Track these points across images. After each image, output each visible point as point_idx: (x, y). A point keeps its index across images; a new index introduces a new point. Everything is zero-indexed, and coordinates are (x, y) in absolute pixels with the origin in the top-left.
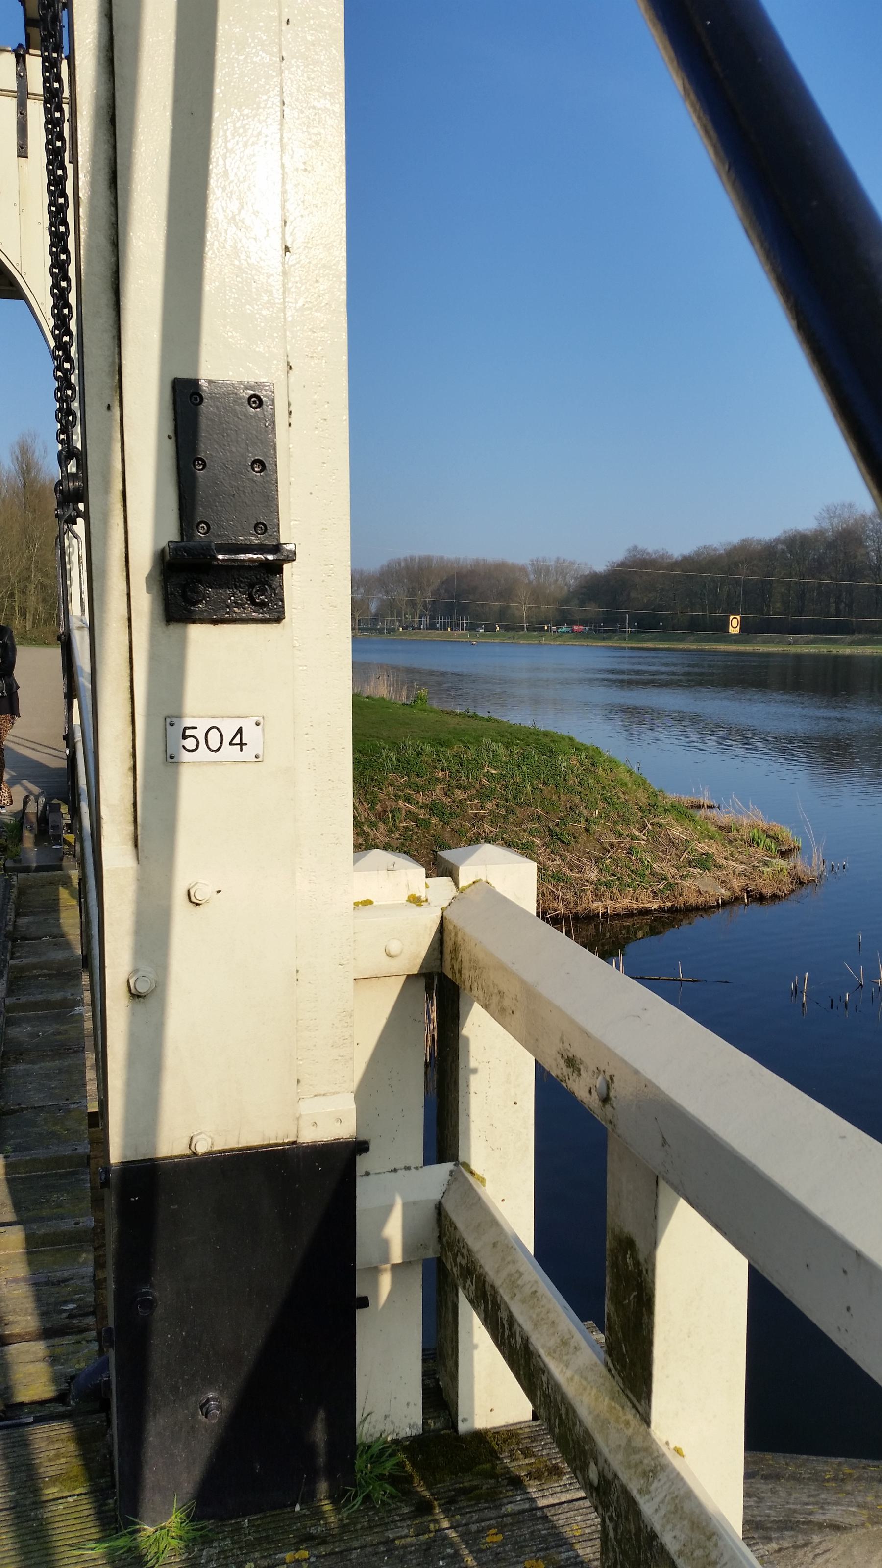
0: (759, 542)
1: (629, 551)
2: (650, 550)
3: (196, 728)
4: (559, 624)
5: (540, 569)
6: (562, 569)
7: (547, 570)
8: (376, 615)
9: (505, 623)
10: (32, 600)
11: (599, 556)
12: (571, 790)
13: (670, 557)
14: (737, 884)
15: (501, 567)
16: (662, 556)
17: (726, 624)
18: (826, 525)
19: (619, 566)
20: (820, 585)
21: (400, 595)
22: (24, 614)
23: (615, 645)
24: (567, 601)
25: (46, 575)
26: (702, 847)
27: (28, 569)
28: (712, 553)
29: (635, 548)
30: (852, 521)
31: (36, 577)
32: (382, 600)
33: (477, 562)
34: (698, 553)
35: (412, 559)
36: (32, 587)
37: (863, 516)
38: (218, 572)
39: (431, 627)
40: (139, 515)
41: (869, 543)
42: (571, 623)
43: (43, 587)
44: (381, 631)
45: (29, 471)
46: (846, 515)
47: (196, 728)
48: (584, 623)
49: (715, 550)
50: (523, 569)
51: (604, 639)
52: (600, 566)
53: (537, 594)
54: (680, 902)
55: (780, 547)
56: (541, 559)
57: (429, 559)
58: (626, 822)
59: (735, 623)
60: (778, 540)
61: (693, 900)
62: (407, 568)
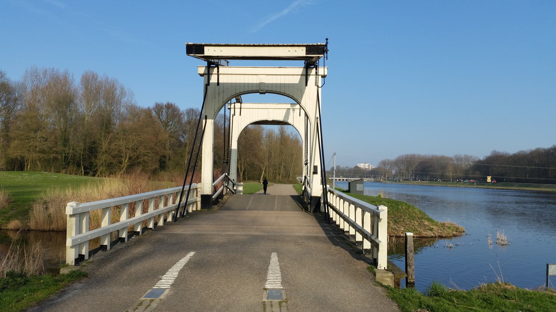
0: (544, 149)
1: (492, 152)
4: (464, 179)
5: (459, 159)
6: (467, 158)
8: (395, 175)
9: (445, 179)
10: (282, 171)
11: (481, 153)
12: (401, 213)
14: (437, 234)
15: (443, 158)
17: (486, 179)
21: (403, 167)
22: (279, 175)
23: (517, 188)
24: (468, 170)
25: (286, 163)
26: (432, 227)
27: (281, 162)
29: (495, 151)
31: (283, 164)
32: (396, 170)
33: (433, 156)
35: (408, 155)
38: (315, 172)
39: (415, 180)
40: (312, 170)
42: (469, 179)
43: (285, 166)
44: (396, 181)
48: (474, 179)
50: (451, 159)
51: (482, 185)
52: (482, 158)
53: (456, 168)
54: (421, 236)
57: (414, 155)
58: (413, 220)
59: (489, 179)
61: (424, 235)
62: (406, 158)
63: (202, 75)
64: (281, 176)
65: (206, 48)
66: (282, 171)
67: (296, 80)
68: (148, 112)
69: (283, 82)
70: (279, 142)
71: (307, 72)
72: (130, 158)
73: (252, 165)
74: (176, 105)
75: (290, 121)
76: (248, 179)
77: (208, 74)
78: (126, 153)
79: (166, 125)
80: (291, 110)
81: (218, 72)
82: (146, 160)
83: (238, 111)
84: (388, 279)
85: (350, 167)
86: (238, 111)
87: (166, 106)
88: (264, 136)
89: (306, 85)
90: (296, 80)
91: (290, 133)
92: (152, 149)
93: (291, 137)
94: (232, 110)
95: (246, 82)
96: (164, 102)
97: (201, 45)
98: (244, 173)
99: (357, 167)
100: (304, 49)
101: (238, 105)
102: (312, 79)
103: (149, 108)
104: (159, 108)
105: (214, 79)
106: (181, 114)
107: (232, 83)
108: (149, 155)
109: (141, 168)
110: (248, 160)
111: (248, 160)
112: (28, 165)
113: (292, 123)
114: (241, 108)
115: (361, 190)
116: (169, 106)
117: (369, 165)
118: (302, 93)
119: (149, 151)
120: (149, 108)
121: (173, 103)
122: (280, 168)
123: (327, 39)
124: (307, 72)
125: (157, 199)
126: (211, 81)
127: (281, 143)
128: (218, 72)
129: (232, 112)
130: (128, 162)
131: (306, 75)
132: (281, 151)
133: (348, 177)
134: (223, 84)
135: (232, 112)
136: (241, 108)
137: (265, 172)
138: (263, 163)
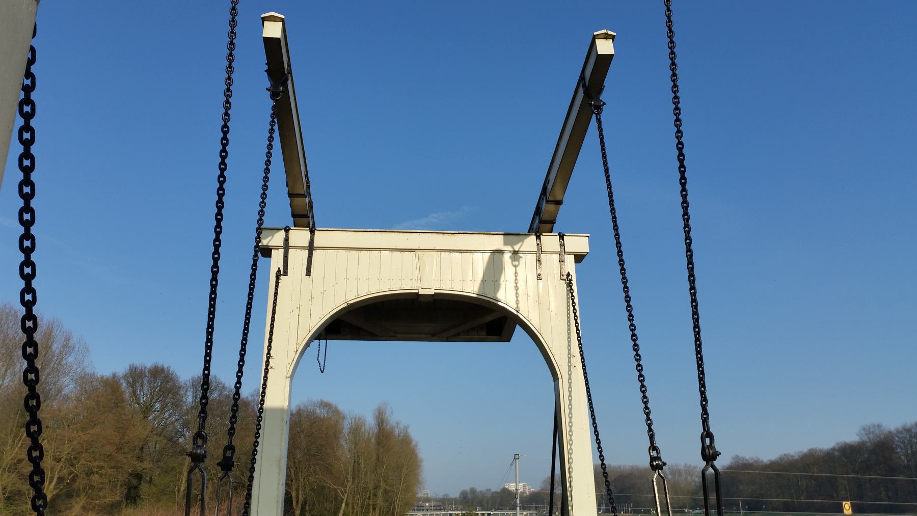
0: (821, 451)
2: (747, 458)
3: (308, 273)
7: (679, 471)
10: (380, 501)
13: (762, 462)
16: (756, 461)
18: (865, 438)
19: (727, 468)
20: (871, 479)
22: (374, 509)
27: (379, 481)
28: (791, 459)
29: (737, 456)
30: (882, 437)
33: (632, 468)
34: (781, 459)
36: (380, 492)
37: (890, 432)
41: (899, 450)
45: (382, 423)
46: (877, 432)
47: (308, 273)
49: (792, 456)
55: (836, 453)
56: (401, 425)
60: (833, 449)
64: (377, 511)
66: (380, 501)
68: (112, 384)
70: (373, 440)
72: (61, 479)
73: (320, 491)
74: (172, 369)
78: (52, 469)
79: (147, 409)
80: (507, 257)
82: (94, 484)
83: (298, 259)
85: (493, 490)
86: (298, 259)
87: (150, 371)
88: (346, 431)
91: (395, 424)
92: (110, 457)
93: (397, 432)
94: (277, 258)
96: (147, 361)
98: (303, 508)
99: (505, 491)
101: (300, 237)
103: (114, 375)
104: (135, 375)
106: (180, 387)
108: (103, 471)
109: (82, 501)
110: (312, 479)
111: (312, 479)
114: (311, 248)
116: (158, 373)
117: (524, 486)
119: (102, 464)
120: (114, 375)
121: (165, 366)
122: (375, 495)
130: (55, 489)
132: (378, 458)
133: (491, 510)
136: (311, 248)
137: (347, 504)
138: (343, 485)
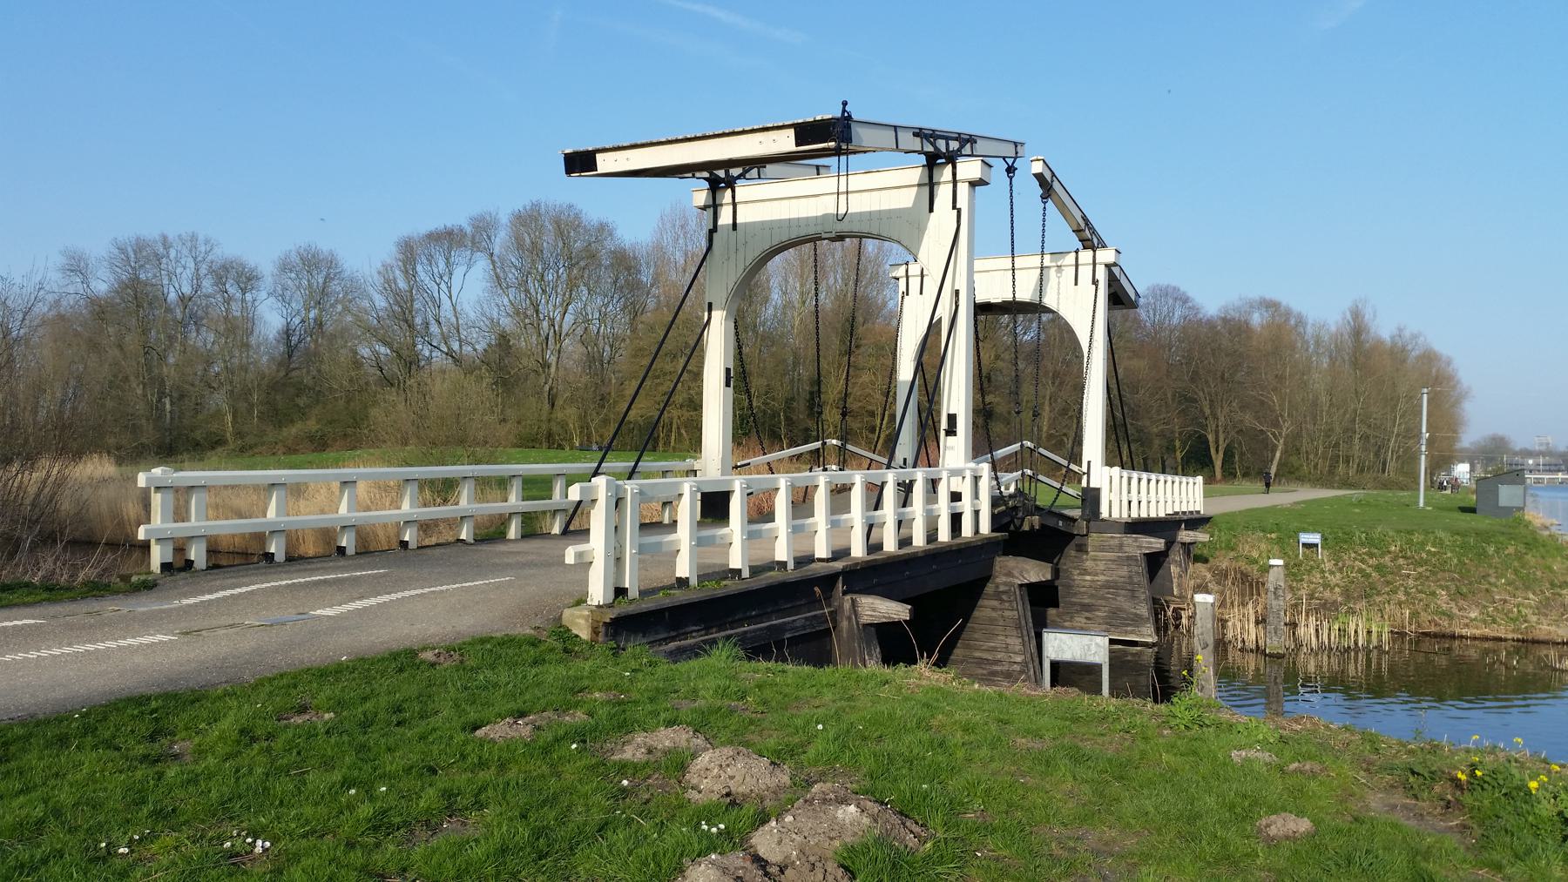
38: (951, 432)
61: (1542, 637)
63: (704, 208)
65: (599, 157)
67: (906, 199)
69: (875, 208)
71: (931, 177)
75: (1049, 301)
76: (1245, 475)
77: (714, 206)
81: (954, 175)
84: (582, 621)
89: (931, 210)
90: (906, 199)
94: (902, 282)
95: (794, 215)
97: (588, 152)
100: (791, 132)
102: (943, 193)
105: (725, 218)
107: (763, 223)
112: (668, 436)
113: (1053, 306)
115: (1517, 503)
118: (920, 229)
123: (845, 104)
124: (931, 177)
125: (483, 483)
126: (720, 222)
127: (1355, 364)
128: (954, 175)
129: (902, 287)
131: (931, 185)
134: (746, 224)
135: (902, 287)
136: (1077, 266)
